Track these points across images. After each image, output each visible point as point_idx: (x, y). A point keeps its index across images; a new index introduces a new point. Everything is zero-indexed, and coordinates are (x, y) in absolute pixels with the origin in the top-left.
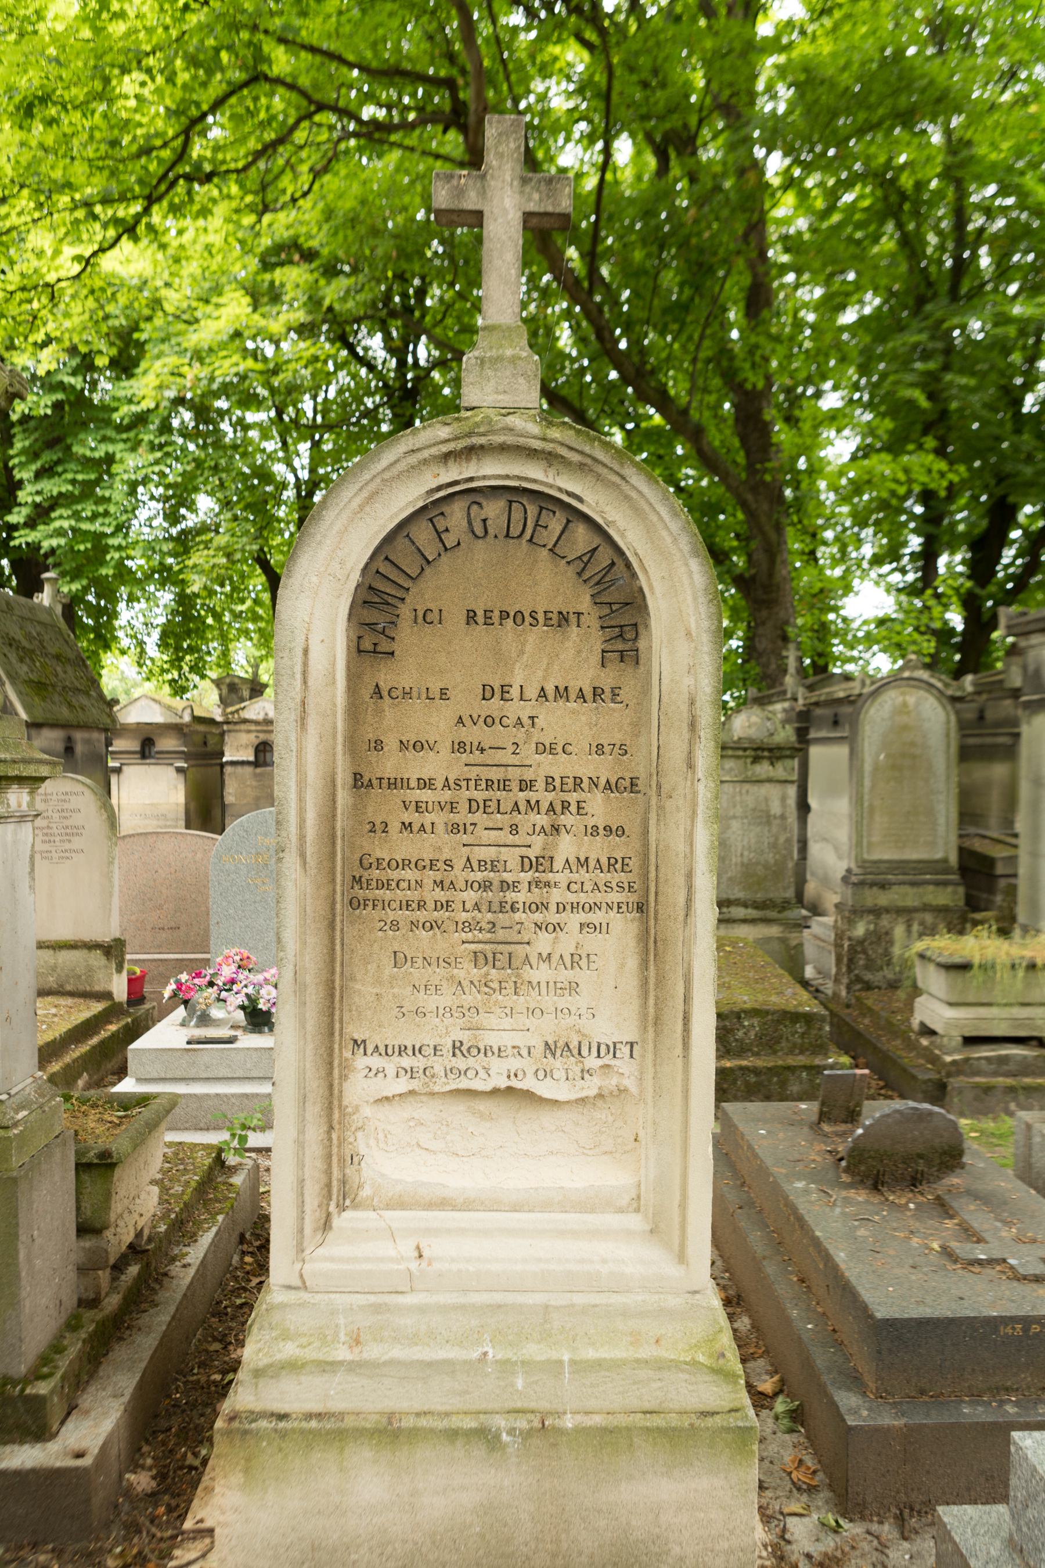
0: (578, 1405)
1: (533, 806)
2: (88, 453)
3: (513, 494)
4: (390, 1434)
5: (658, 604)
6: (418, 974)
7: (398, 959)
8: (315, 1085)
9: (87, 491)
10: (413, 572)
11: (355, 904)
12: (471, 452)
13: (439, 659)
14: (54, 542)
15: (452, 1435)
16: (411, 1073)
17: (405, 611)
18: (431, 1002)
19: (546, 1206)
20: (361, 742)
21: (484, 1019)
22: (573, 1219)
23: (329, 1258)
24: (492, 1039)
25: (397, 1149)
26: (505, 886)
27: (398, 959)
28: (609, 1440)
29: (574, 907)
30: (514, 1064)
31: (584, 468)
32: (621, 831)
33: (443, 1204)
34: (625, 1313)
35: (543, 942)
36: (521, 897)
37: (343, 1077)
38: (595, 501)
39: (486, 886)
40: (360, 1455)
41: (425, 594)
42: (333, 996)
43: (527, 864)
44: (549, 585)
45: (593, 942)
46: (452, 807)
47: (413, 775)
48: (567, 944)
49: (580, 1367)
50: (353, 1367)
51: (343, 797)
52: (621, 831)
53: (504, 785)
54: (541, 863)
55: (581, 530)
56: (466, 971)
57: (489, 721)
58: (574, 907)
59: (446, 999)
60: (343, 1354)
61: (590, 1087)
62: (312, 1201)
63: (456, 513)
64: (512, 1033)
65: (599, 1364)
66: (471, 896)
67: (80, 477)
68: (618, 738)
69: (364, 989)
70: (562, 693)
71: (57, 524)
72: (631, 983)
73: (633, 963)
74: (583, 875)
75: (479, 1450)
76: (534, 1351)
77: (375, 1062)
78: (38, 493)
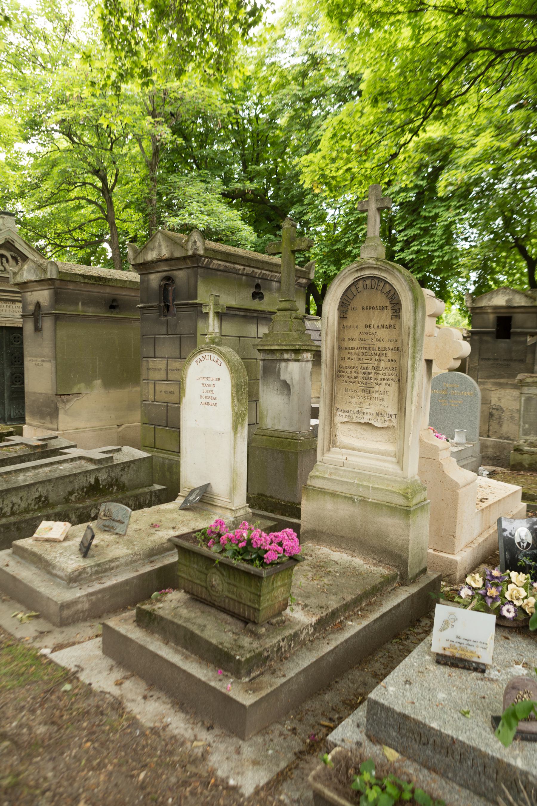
0: (373, 497)
1: (376, 354)
2: (427, 214)
3: (372, 278)
4: (334, 495)
5: (403, 304)
6: (350, 393)
7: (346, 390)
8: (328, 417)
9: (426, 231)
10: (384, 291)
11: (338, 376)
12: (362, 269)
13: (357, 318)
14: (411, 257)
15: (345, 497)
16: (348, 417)
17: (350, 308)
18: (353, 400)
19: (375, 453)
20: (340, 339)
21: (364, 406)
22: (381, 457)
23: (328, 457)
24: (365, 410)
25: (346, 435)
26: (369, 374)
27: (346, 390)
28: (377, 506)
29: (384, 379)
30: (369, 417)
31: (386, 271)
32: (395, 361)
33: (353, 449)
34: (387, 479)
35: (377, 388)
36: (372, 376)
37: (334, 416)
38: (389, 278)
39: (365, 373)
40: (328, 498)
41: (354, 304)
42: (333, 397)
43: (374, 368)
44: (380, 300)
45: (388, 388)
46: (358, 354)
47: (350, 346)
48: (382, 389)
49: (374, 489)
50: (328, 479)
51: (336, 351)
52: (395, 361)
53: (369, 349)
54: (377, 368)
55: (387, 285)
56: (360, 394)
57: (367, 333)
58: (384, 379)
59: (355, 400)
60: (327, 476)
61: (386, 425)
62: (326, 444)
63: (360, 284)
64: (370, 410)
65: (377, 489)
66: (362, 375)
67: (423, 226)
68: (395, 337)
69: (339, 396)
70: (382, 326)
71: (412, 249)
72: (396, 399)
73: (397, 394)
74: (386, 372)
75: (351, 502)
76: (365, 483)
77: (341, 413)
78: (406, 236)
